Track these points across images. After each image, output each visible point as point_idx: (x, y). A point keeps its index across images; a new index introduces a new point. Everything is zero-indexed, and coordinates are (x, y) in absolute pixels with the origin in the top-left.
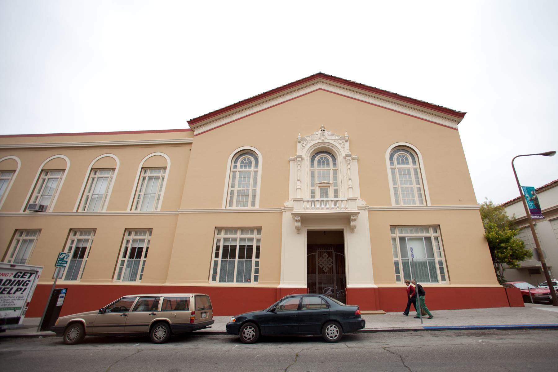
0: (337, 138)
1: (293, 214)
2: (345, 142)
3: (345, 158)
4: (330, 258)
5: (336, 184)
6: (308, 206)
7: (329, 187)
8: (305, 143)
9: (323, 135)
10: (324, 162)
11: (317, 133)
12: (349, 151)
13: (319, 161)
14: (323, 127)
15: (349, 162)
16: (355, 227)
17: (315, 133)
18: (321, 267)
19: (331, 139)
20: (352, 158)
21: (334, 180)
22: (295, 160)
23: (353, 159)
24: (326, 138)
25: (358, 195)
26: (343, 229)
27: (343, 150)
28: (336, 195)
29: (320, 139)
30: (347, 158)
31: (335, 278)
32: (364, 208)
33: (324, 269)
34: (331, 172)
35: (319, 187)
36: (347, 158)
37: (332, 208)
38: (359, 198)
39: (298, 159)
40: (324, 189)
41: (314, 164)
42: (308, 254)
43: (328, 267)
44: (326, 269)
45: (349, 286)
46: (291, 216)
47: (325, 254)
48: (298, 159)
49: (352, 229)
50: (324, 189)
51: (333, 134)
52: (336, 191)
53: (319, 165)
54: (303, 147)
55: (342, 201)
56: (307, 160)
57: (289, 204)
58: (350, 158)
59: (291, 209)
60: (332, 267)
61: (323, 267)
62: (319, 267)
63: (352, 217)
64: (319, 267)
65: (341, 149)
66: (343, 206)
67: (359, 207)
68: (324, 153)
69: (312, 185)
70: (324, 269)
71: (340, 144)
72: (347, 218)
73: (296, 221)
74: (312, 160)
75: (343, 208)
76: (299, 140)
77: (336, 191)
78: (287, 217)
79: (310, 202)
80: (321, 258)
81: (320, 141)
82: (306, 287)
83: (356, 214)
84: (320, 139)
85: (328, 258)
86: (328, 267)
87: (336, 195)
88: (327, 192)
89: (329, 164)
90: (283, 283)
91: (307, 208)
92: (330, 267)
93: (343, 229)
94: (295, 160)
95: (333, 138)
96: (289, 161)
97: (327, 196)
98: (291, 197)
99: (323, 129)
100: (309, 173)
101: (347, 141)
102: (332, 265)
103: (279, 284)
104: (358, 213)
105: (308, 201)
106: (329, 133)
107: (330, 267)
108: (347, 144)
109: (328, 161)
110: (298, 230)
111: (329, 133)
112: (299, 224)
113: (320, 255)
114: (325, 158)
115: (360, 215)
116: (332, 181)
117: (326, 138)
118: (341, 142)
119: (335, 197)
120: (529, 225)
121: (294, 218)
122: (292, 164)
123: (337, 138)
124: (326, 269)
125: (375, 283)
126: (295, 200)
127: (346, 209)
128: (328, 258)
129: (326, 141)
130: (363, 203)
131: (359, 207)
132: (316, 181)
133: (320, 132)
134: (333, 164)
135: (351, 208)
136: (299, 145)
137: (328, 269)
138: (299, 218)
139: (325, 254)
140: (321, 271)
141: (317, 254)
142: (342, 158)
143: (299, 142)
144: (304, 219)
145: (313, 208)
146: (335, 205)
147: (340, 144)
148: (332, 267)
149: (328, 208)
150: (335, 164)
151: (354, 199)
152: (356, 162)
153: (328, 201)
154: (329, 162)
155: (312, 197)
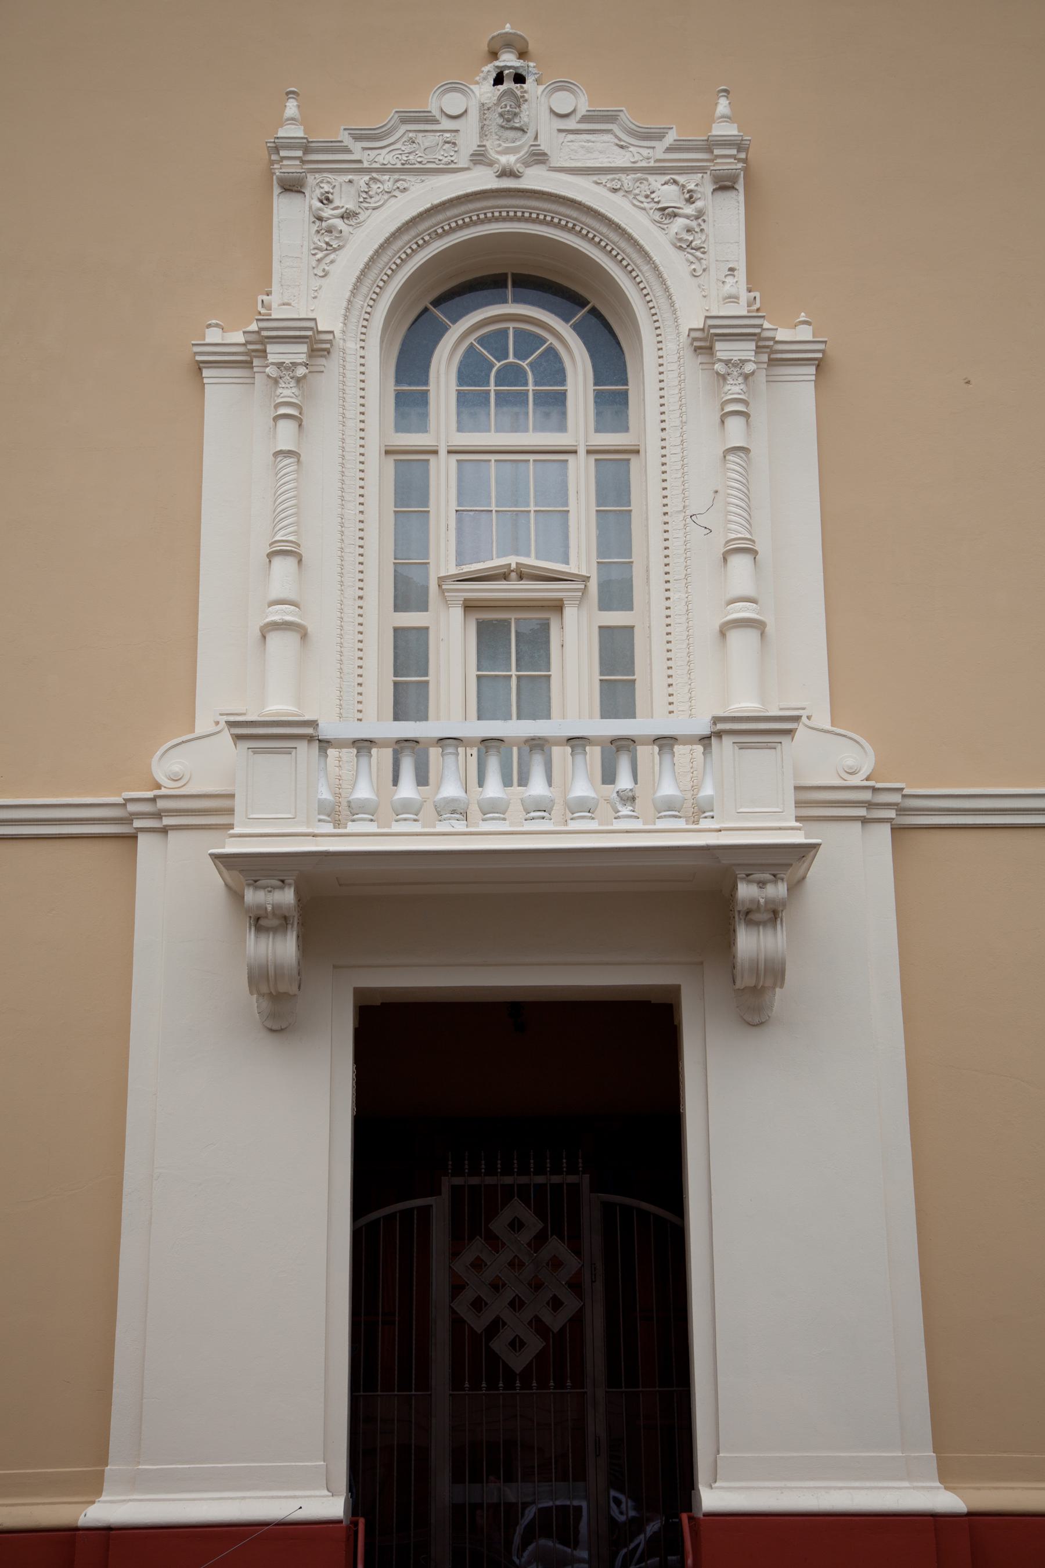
0: (639, 154)
1: (224, 861)
2: (707, 199)
3: (704, 344)
4: (556, 1246)
5: (616, 592)
6: (363, 792)
7: (557, 607)
8: (345, 201)
9: (510, 121)
10: (512, 375)
11: (453, 103)
12: (738, 285)
13: (471, 371)
14: (510, 42)
15: (734, 388)
16: (774, 972)
17: (433, 106)
18: (479, 1323)
19: (579, 158)
20: (763, 344)
21: (604, 547)
22: (249, 358)
23: (775, 358)
24: (538, 158)
25: (807, 690)
26: (676, 990)
27: (688, 275)
28: (617, 695)
29: (479, 158)
30: (723, 350)
31: (596, 1425)
32: (863, 806)
33: (499, 1345)
34: (581, 474)
35: (469, 607)
36: (723, 350)
37: (585, 808)
38: (823, 719)
39: (285, 354)
40: (512, 632)
41: (422, 399)
42: (359, 1208)
43: (539, 1326)
44: (517, 1344)
45: (714, 1497)
46: (214, 879)
47: (517, 1209)
48: (285, 354)
49: (754, 998)
50: (512, 632)
51: (598, 120)
52: (617, 651)
53: (470, 404)
54: (328, 241)
55: (665, 742)
56: (364, 361)
57: (193, 763)
58: (745, 350)
59: (214, 811)
60: (577, 1321)
61: (495, 1326)
62: (457, 1322)
63: (745, 891)
64: (457, 1322)
65: (673, 264)
66: (668, 789)
67: (811, 803)
68: (514, 290)
69: (408, 594)
70: (499, 1345)
71: (668, 213)
72: (707, 898)
73: (260, 922)
74: (411, 363)
75: (670, 807)
76: (291, 168)
77: (617, 651)
78: (174, 888)
79: (594, 753)
80: (476, 1248)
81: (483, 179)
82: (329, 1504)
83: (786, 861)
84: (479, 158)
85: (539, 1240)
86: (539, 1326)
87: (617, 695)
88: (536, 645)
89: (559, 400)
90: (136, 1483)
91: (356, 810)
92: (555, 1322)
93: (676, 990)
94: (249, 358)
95: (603, 150)
96: (199, 367)
97: (536, 700)
98: (217, 698)
99: (508, 60)
100: (379, 477)
101: (724, 185)
102: (571, 1305)
103: (92, 1486)
104: (805, 852)
105: (363, 745)
106: (563, 102)
107: (555, 1322)
108: (728, 217)
109: (552, 369)
110: (279, 1006)
111: (563, 102)
112: (285, 948)
113: (471, 1221)
114: (528, 342)
115: (817, 870)
116: (582, 558)
117: (538, 158)
118: (669, 195)
119: (608, 712)
120: (515, 750)
121: (236, 895)
122: (220, 393)
123: (639, 154)
124: (517, 1344)
125: (948, 1475)
126: (249, 733)
127: (701, 810)
128: (539, 1240)
129: (535, 179)
130: (842, 759)
131: (811, 803)
132: (443, 560)
133: (485, 91)
134: (600, 398)
135: (741, 809)
136: (290, 217)
137: (535, 1344)
138: (287, 897)
139: (517, 1209)
140: (476, 1360)
141: (439, 1206)
142: (675, 344)
143: (293, 187)
144: (327, 903)
145: (405, 809)
146: (609, 776)
147: (668, 213)
148: (577, 1321)
149: (541, 808)
150: (613, 401)
151: (769, 731)
152: (800, 391)
153: (537, 744)
154: (559, 375)
155: (408, 701)
